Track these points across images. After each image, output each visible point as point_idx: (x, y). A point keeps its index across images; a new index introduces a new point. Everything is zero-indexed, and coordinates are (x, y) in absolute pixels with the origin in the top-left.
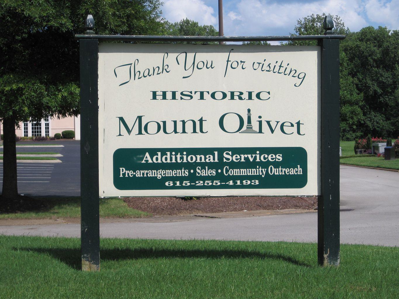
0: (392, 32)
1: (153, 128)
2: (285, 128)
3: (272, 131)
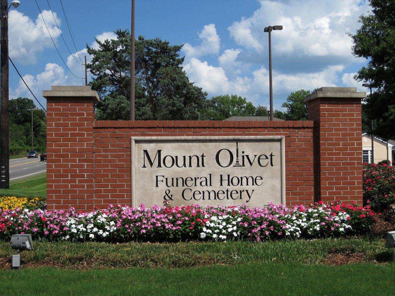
1: (235, 181)
3: (251, 164)
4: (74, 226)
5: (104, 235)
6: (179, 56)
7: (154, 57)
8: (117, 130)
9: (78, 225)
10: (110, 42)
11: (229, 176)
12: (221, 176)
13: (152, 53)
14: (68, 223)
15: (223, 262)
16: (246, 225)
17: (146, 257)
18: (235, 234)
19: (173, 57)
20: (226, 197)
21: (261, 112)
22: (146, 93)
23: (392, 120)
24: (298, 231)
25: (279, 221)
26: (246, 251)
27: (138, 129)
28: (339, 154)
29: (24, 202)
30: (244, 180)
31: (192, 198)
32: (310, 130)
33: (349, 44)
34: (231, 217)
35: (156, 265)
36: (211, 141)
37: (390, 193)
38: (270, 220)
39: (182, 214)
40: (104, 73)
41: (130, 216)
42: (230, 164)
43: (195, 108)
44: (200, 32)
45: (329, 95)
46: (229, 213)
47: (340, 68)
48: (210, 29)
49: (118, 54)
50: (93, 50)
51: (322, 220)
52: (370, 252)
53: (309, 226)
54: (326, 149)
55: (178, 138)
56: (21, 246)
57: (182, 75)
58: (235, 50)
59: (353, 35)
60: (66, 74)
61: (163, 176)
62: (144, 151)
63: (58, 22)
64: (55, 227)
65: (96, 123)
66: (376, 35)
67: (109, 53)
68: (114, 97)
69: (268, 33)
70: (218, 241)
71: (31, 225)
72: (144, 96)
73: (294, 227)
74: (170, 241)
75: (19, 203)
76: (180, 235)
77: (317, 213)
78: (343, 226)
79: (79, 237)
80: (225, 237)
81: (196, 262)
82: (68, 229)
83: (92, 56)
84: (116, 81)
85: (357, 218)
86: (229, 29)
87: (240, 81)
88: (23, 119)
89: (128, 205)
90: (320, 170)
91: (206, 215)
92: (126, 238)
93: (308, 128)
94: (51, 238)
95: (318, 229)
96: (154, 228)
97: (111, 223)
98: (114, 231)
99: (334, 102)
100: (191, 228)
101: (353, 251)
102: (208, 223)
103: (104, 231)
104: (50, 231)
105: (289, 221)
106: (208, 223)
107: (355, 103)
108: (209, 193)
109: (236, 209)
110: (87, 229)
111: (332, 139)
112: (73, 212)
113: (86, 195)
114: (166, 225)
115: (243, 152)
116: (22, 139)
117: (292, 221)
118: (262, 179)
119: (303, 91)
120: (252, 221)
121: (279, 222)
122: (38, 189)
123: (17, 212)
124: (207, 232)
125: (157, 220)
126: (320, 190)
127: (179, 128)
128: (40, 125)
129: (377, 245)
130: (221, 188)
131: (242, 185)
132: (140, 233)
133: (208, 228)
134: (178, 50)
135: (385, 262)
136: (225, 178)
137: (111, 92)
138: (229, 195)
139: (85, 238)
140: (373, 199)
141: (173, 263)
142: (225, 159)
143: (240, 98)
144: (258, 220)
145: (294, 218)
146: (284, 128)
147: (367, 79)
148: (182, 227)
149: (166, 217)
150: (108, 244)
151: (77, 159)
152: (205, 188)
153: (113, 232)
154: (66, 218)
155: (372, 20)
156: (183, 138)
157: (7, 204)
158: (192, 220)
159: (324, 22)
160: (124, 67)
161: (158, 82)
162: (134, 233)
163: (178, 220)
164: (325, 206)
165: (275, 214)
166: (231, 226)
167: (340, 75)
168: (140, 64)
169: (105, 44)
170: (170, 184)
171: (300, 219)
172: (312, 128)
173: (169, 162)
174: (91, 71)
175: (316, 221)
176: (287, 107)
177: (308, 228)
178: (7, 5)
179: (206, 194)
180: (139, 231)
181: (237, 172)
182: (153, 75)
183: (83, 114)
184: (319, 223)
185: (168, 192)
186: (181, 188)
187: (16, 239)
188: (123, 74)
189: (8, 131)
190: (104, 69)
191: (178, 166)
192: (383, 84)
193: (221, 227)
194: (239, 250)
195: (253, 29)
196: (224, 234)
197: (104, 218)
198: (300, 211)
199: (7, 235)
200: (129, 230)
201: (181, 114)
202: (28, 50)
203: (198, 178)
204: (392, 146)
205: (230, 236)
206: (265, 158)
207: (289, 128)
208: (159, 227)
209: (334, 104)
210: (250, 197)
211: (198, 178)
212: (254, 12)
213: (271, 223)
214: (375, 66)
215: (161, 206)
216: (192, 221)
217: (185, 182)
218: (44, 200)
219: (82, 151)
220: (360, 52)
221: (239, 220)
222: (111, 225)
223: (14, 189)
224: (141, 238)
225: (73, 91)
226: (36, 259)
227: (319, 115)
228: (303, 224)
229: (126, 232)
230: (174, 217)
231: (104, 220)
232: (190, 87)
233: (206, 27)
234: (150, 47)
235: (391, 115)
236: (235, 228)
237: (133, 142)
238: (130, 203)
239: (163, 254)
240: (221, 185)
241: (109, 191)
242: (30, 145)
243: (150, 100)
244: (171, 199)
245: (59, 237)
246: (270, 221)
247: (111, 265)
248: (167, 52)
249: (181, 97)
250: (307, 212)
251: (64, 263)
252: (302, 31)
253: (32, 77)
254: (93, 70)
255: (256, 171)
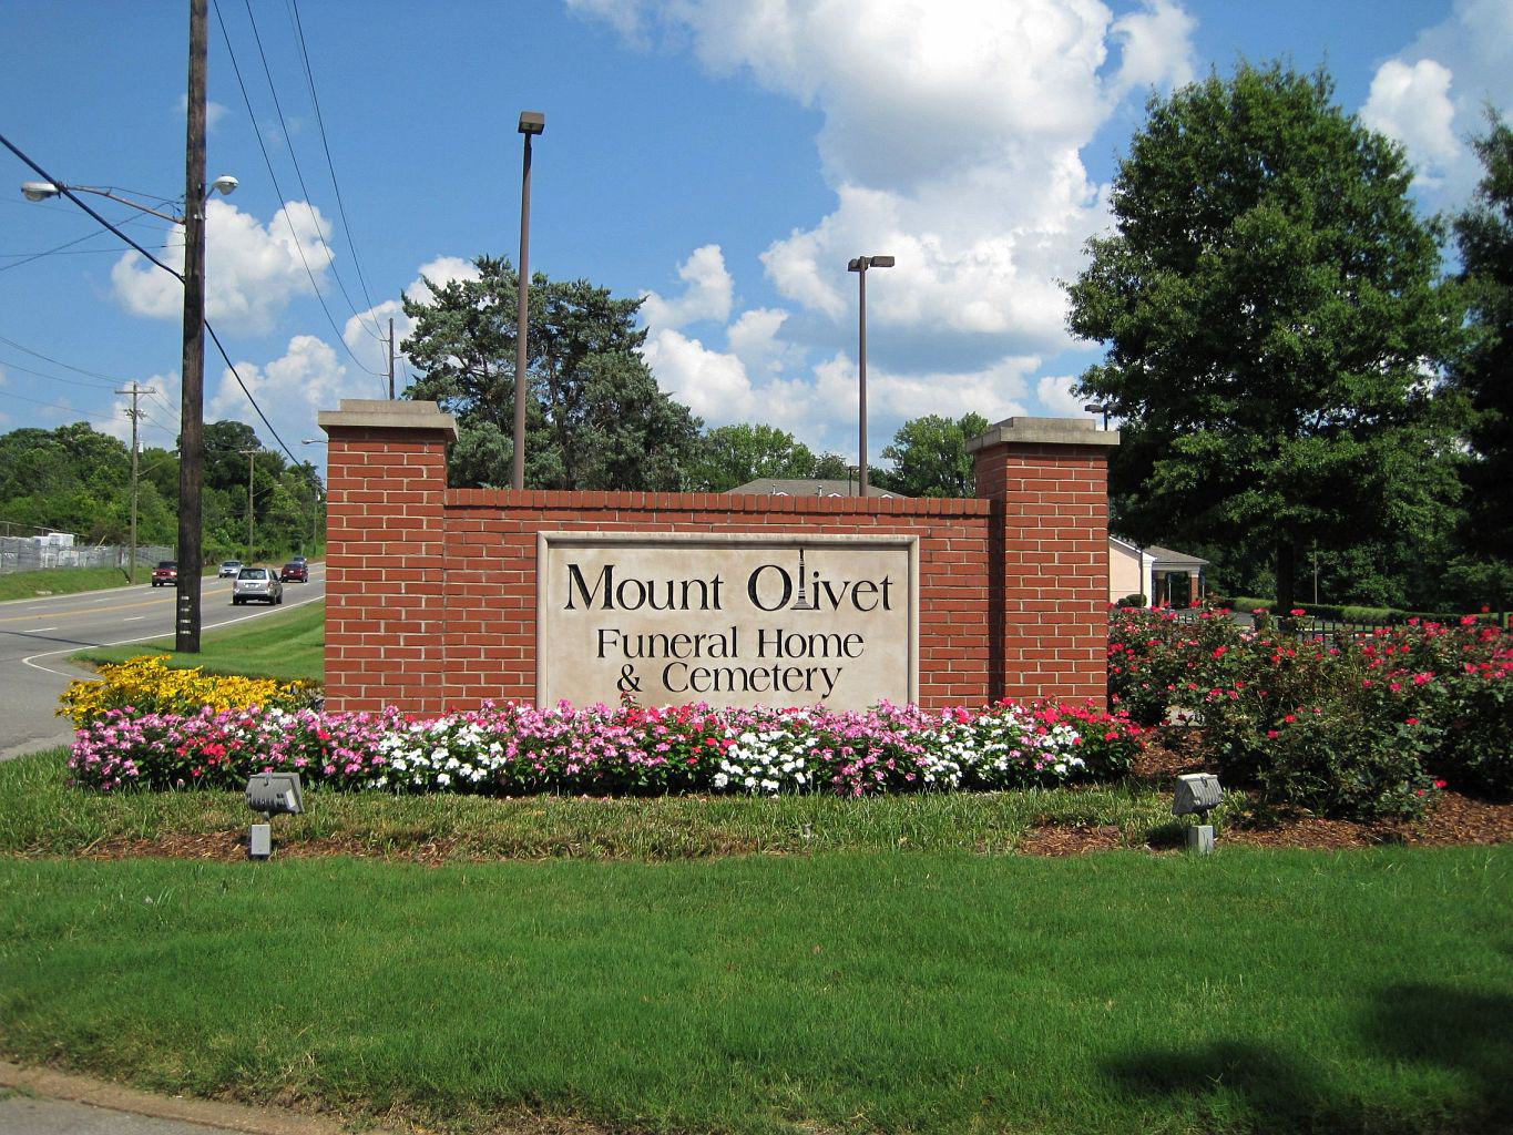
0: (1490, 175)
1: (796, 645)
2: (860, 596)
3: (835, 603)
4: (398, 753)
5: (476, 777)
6: (633, 326)
7: (572, 327)
8: (503, 513)
9: (408, 750)
10: (460, 286)
11: (780, 632)
12: (761, 632)
13: (566, 318)
14: (384, 746)
15: (777, 848)
16: (828, 756)
17: (586, 833)
18: (800, 778)
19: (618, 329)
20: (713, 684)
21: (831, 470)
22: (550, 418)
23: (1161, 497)
24: (955, 772)
25: (909, 745)
26: (832, 819)
27: (556, 513)
28: (1050, 583)
29: (269, 692)
30: (818, 643)
31: (687, 687)
32: (982, 521)
33: (1060, 307)
34: (790, 735)
35: (612, 853)
36: (737, 545)
37: (1180, 681)
38: (886, 744)
39: (668, 726)
40: (445, 364)
41: (539, 730)
42: (783, 603)
43: (672, 456)
44: (684, 264)
45: (1030, 436)
46: (785, 726)
47: (1031, 363)
48: (709, 257)
49: (482, 317)
50: (419, 306)
51: (1014, 744)
52: (1133, 825)
53: (980, 760)
54: (1018, 570)
55: (656, 535)
56: (273, 802)
57: (640, 373)
58: (768, 311)
59: (1070, 285)
60: (340, 362)
61: (617, 631)
62: (570, 566)
63: (325, 229)
64: (351, 754)
65: (451, 497)
66: (1126, 287)
67: (458, 315)
68: (467, 426)
69: (858, 273)
70: (760, 794)
71: (290, 750)
72: (544, 425)
73: (945, 763)
74: (640, 792)
75: (256, 694)
76: (665, 780)
77: (1000, 726)
78: (1065, 760)
79: (412, 782)
80: (775, 785)
81: (709, 847)
82: (383, 760)
83: (415, 321)
84: (474, 385)
85: (1098, 740)
86: (764, 257)
87: (783, 389)
88: (228, 476)
89: (529, 702)
90: (1004, 622)
91: (729, 729)
92: (529, 784)
93: (976, 516)
94: (341, 783)
95: (1003, 767)
96: (600, 761)
97: (492, 745)
98: (501, 767)
99: (1041, 455)
100: (692, 761)
101: (1091, 821)
102: (734, 750)
103: (475, 767)
104: (340, 767)
105: (932, 745)
106: (734, 750)
107: (1092, 457)
108: (731, 674)
109: (803, 716)
110: (432, 762)
111: (1034, 546)
112: (395, 719)
113: (423, 674)
114: (630, 753)
115: (816, 574)
116: (224, 526)
117: (940, 747)
118: (861, 640)
119: (934, 418)
120: (843, 745)
121: (908, 749)
122: (271, 656)
123: (254, 716)
124: (732, 772)
125: (607, 740)
126: (1003, 669)
127: (658, 510)
128: (270, 492)
129: (1149, 807)
130: (761, 663)
131: (811, 654)
132: (565, 772)
133: (732, 762)
134: (633, 310)
135: (1170, 848)
136: (771, 636)
137: (461, 413)
138: (780, 679)
139: (426, 783)
140: (1128, 693)
141: (654, 848)
142: (770, 590)
143: (778, 432)
144: (857, 744)
145: (944, 738)
146: (917, 515)
147: (1101, 396)
148: (668, 759)
149: (628, 735)
150: (485, 801)
151: (403, 584)
152: (720, 663)
153: (496, 770)
154: (380, 734)
155: (1117, 249)
156: (667, 535)
157: (225, 696)
158: (695, 742)
159: (997, 249)
160: (494, 350)
161: (581, 389)
162: (549, 772)
163: (660, 741)
164: (1019, 711)
165: (897, 729)
166: (790, 758)
167: (1032, 380)
168: (535, 343)
169: (449, 291)
170: (633, 649)
171: (960, 741)
172: (988, 516)
173: (633, 595)
174: (412, 358)
175: (997, 746)
176: (893, 457)
177: (978, 764)
178: (203, 186)
179: (723, 677)
180: (562, 768)
181: (799, 623)
182: (568, 372)
183: (419, 473)
184: (1006, 752)
185: (627, 671)
186: (660, 661)
187: (261, 786)
188: (492, 368)
189: (199, 505)
190: (444, 353)
191: (654, 606)
192: (1141, 408)
193: (766, 759)
194: (813, 817)
195: (823, 262)
196: (772, 778)
197: (476, 733)
198: (959, 723)
199: (228, 773)
200: (537, 766)
201: (638, 471)
202: (250, 301)
203: (704, 636)
204: (1154, 559)
205: (787, 782)
206: (869, 588)
207: (930, 516)
208: (612, 758)
209: (1073, 459)
210: (831, 686)
211: (704, 636)
212: (822, 216)
213: (889, 751)
214: (1120, 362)
215: (615, 706)
216: (695, 745)
217: (670, 646)
218: (315, 685)
219: (415, 564)
220: (1088, 327)
221: (811, 742)
222: (493, 751)
223: (210, 654)
224: (565, 785)
225: (395, 413)
226: (309, 835)
227: (1004, 485)
228: (966, 755)
229: (529, 770)
230: (649, 734)
231: (476, 739)
232: (661, 404)
233: (699, 252)
234: (561, 302)
235: (1160, 483)
236: (801, 763)
237: (544, 545)
238: (532, 696)
239: (628, 826)
240: (761, 654)
241: (481, 666)
242: (245, 542)
243: (561, 435)
244: (635, 687)
245: (360, 780)
246: (885, 747)
247: (500, 852)
248: (605, 316)
249: (637, 429)
250: (976, 724)
251: (379, 847)
252: (946, 269)
253: (254, 369)
254: (418, 356)
255: (845, 620)
